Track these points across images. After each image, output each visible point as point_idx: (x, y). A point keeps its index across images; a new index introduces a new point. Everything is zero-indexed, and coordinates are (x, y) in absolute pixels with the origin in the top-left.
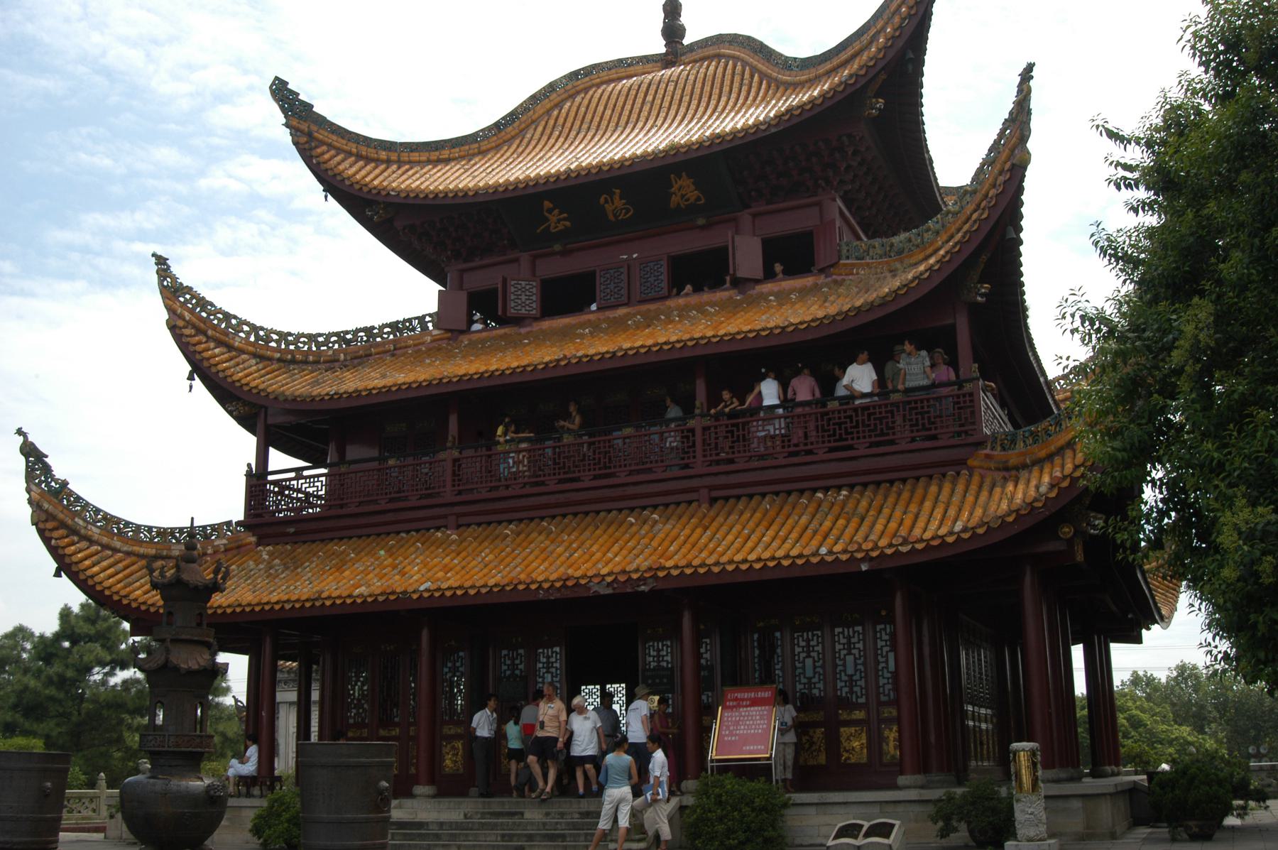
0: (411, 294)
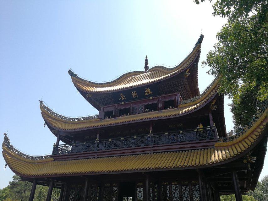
0: (94, 112)
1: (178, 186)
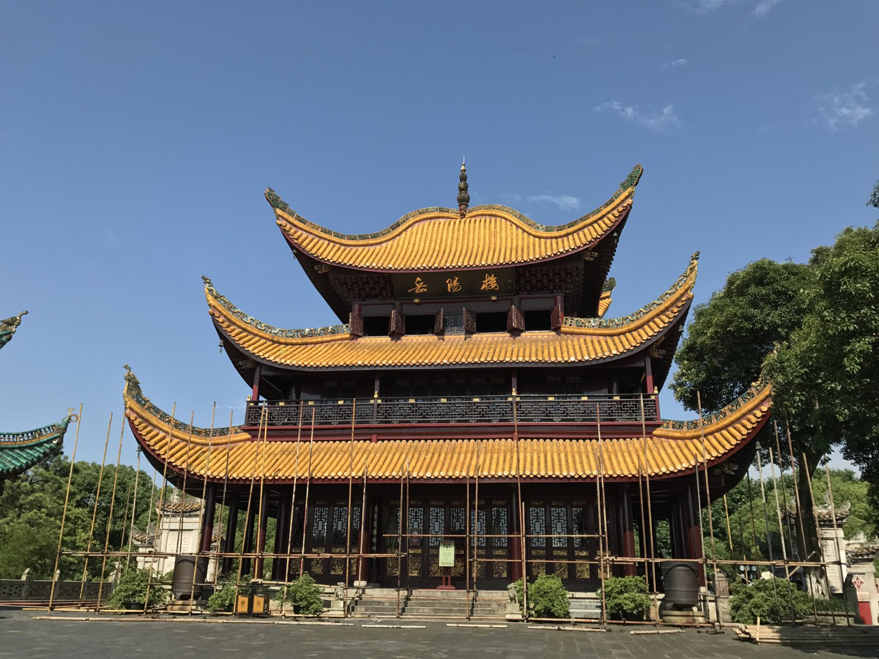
1: (564, 509)
